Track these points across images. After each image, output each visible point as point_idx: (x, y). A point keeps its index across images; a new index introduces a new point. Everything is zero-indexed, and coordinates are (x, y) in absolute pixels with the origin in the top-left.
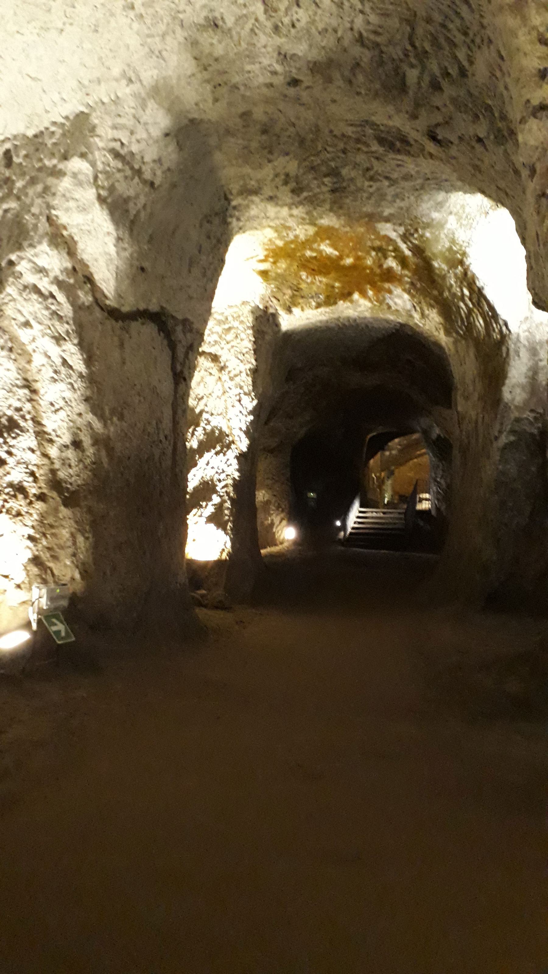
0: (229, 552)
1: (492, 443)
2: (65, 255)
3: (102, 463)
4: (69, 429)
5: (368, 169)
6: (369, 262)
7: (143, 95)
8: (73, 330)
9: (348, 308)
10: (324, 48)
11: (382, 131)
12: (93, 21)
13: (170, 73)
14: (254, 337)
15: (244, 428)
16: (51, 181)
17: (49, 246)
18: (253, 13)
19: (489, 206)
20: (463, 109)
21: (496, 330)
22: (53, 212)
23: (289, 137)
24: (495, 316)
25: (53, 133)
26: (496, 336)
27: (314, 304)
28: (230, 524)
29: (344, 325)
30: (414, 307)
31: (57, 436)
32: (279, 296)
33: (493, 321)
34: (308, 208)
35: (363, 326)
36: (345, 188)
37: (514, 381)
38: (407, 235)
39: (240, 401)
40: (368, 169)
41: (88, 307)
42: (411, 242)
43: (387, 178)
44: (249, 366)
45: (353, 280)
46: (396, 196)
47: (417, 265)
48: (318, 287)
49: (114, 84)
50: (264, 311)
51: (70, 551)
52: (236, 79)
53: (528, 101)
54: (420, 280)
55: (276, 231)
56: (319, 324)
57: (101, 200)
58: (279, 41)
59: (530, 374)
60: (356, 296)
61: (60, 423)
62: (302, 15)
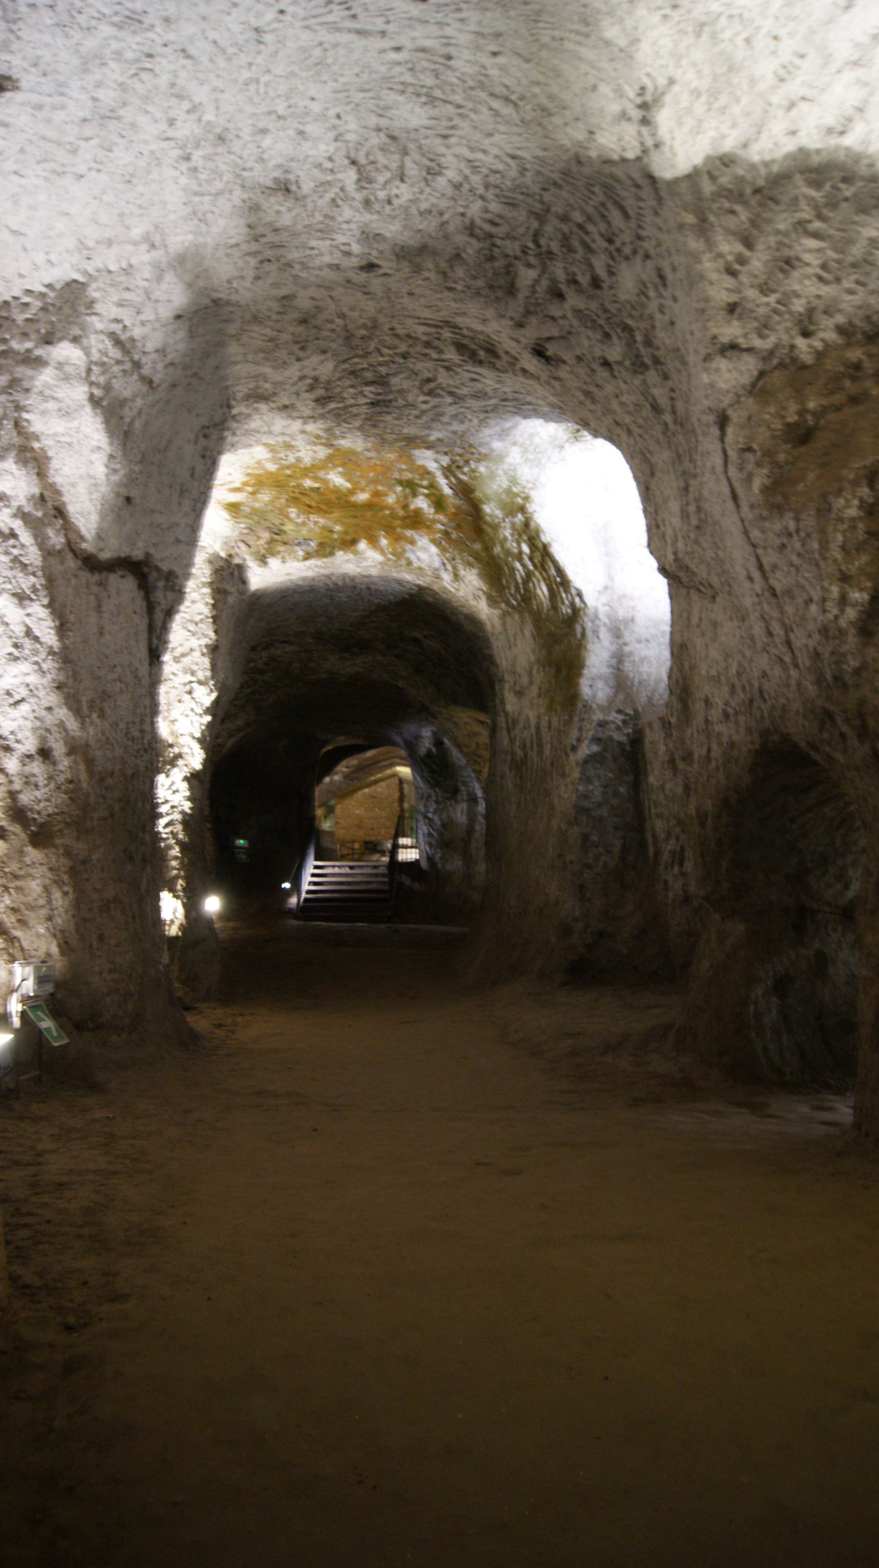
0: (182, 925)
1: (567, 755)
2: (35, 477)
3: (79, 781)
4: (34, 730)
5: (429, 380)
6: (391, 500)
7: (164, 265)
8: (41, 585)
9: (348, 561)
10: (419, 231)
11: (464, 336)
12: (130, 169)
13: (209, 240)
14: (213, 598)
15: (198, 735)
16: (21, 371)
17: (16, 463)
18: (340, 181)
19: (565, 438)
20: (589, 324)
21: (567, 602)
22: (25, 416)
23: (333, 331)
24: (565, 583)
25: (26, 305)
26: (566, 610)
27: (301, 553)
28: (180, 882)
29: (336, 584)
30: (444, 564)
31: (18, 741)
32: (251, 540)
33: (561, 589)
34: (330, 424)
35: (364, 587)
36: (390, 401)
37: (594, 671)
38: (454, 469)
39: (190, 693)
40: (429, 380)
41: (59, 552)
42: (455, 477)
43: (451, 393)
44: (205, 641)
45: (365, 522)
46: (455, 417)
47: (458, 508)
48: (311, 530)
49: (130, 248)
50: (226, 560)
51: (44, 912)
52: (294, 255)
53: (715, 337)
54: (458, 527)
55: (272, 451)
56: (301, 583)
57: (94, 401)
58: (368, 217)
59: (614, 662)
60: (363, 545)
61: (21, 721)
62: (404, 192)
